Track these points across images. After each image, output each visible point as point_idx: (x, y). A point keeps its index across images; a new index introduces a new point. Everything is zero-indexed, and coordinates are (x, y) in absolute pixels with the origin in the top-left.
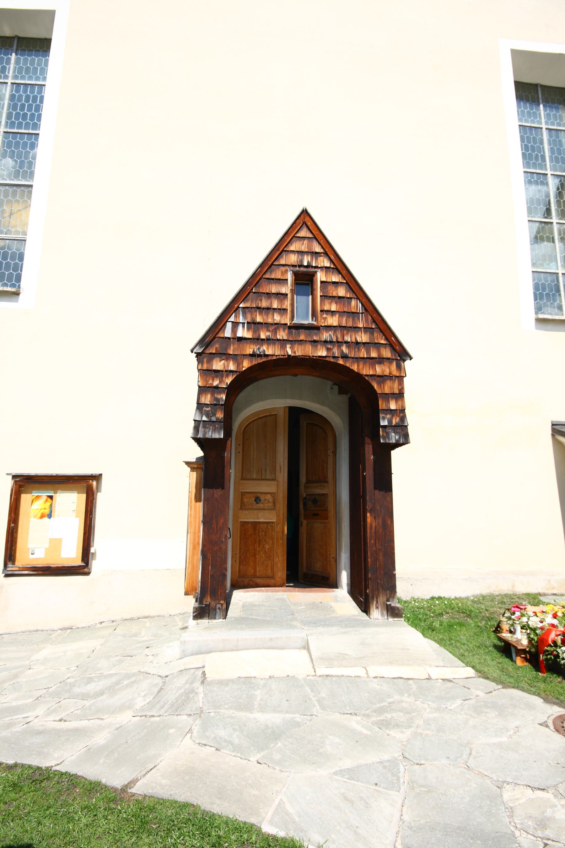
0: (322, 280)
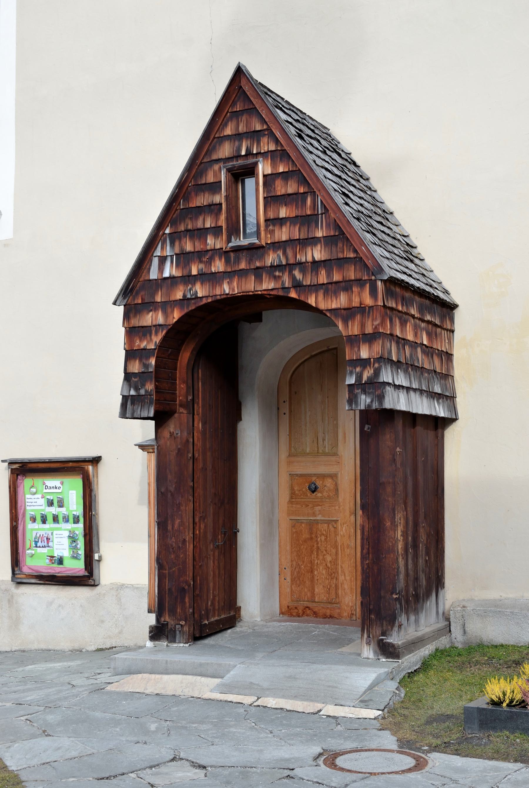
0: (266, 173)
